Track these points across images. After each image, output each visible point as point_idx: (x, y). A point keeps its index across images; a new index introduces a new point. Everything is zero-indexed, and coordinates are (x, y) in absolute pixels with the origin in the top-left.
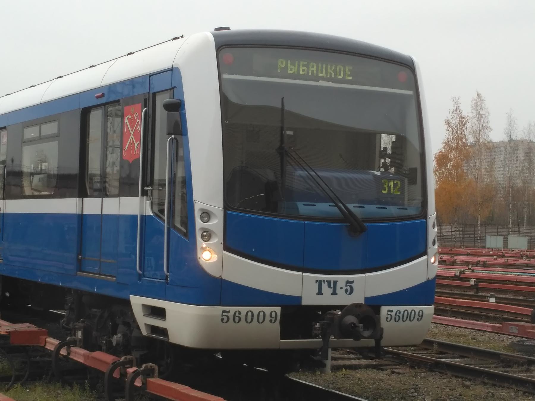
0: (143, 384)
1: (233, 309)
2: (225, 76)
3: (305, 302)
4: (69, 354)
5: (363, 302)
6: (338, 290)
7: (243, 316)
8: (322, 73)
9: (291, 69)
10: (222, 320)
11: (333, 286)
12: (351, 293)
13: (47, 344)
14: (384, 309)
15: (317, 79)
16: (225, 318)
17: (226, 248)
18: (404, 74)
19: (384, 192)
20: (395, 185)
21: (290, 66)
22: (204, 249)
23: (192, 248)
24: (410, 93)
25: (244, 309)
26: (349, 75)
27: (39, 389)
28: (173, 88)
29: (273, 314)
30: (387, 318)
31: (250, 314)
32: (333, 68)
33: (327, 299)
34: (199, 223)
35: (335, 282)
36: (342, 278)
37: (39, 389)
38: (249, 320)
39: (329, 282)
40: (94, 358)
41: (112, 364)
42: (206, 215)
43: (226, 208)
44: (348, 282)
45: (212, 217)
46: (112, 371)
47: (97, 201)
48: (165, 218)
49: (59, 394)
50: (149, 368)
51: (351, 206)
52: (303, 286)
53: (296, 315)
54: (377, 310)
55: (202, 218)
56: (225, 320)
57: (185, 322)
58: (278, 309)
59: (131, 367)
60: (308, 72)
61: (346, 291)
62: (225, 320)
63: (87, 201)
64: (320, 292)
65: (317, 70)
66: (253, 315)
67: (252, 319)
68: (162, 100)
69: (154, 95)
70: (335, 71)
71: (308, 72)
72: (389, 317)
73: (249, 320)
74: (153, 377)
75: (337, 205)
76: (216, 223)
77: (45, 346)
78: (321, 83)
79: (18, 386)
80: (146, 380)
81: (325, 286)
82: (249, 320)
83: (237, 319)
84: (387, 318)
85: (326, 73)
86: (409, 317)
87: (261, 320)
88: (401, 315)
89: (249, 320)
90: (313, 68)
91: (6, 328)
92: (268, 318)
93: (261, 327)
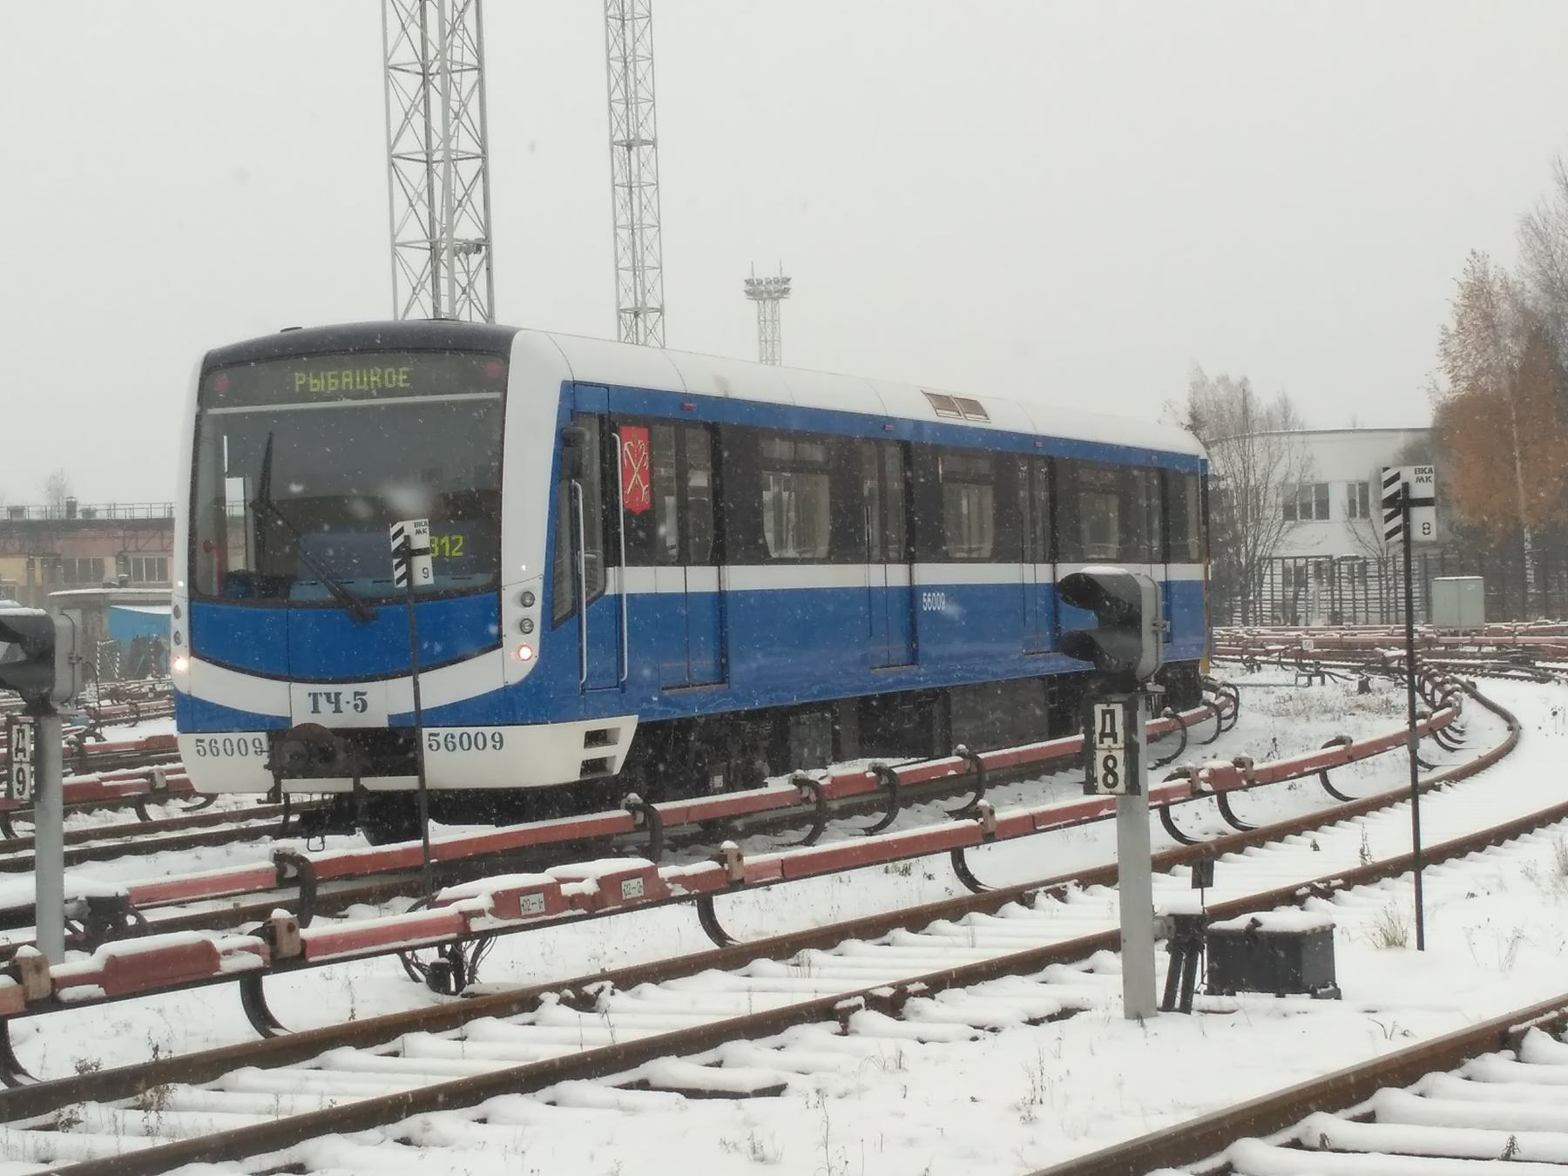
6: (343, 705)
35: (337, 695)
39: (328, 695)
44: (356, 694)
47: (1029, 580)
54: (830, 553)
61: (356, 706)
63: (713, 588)
64: (316, 710)
70: (382, 378)
81: (322, 700)
90: (347, 378)
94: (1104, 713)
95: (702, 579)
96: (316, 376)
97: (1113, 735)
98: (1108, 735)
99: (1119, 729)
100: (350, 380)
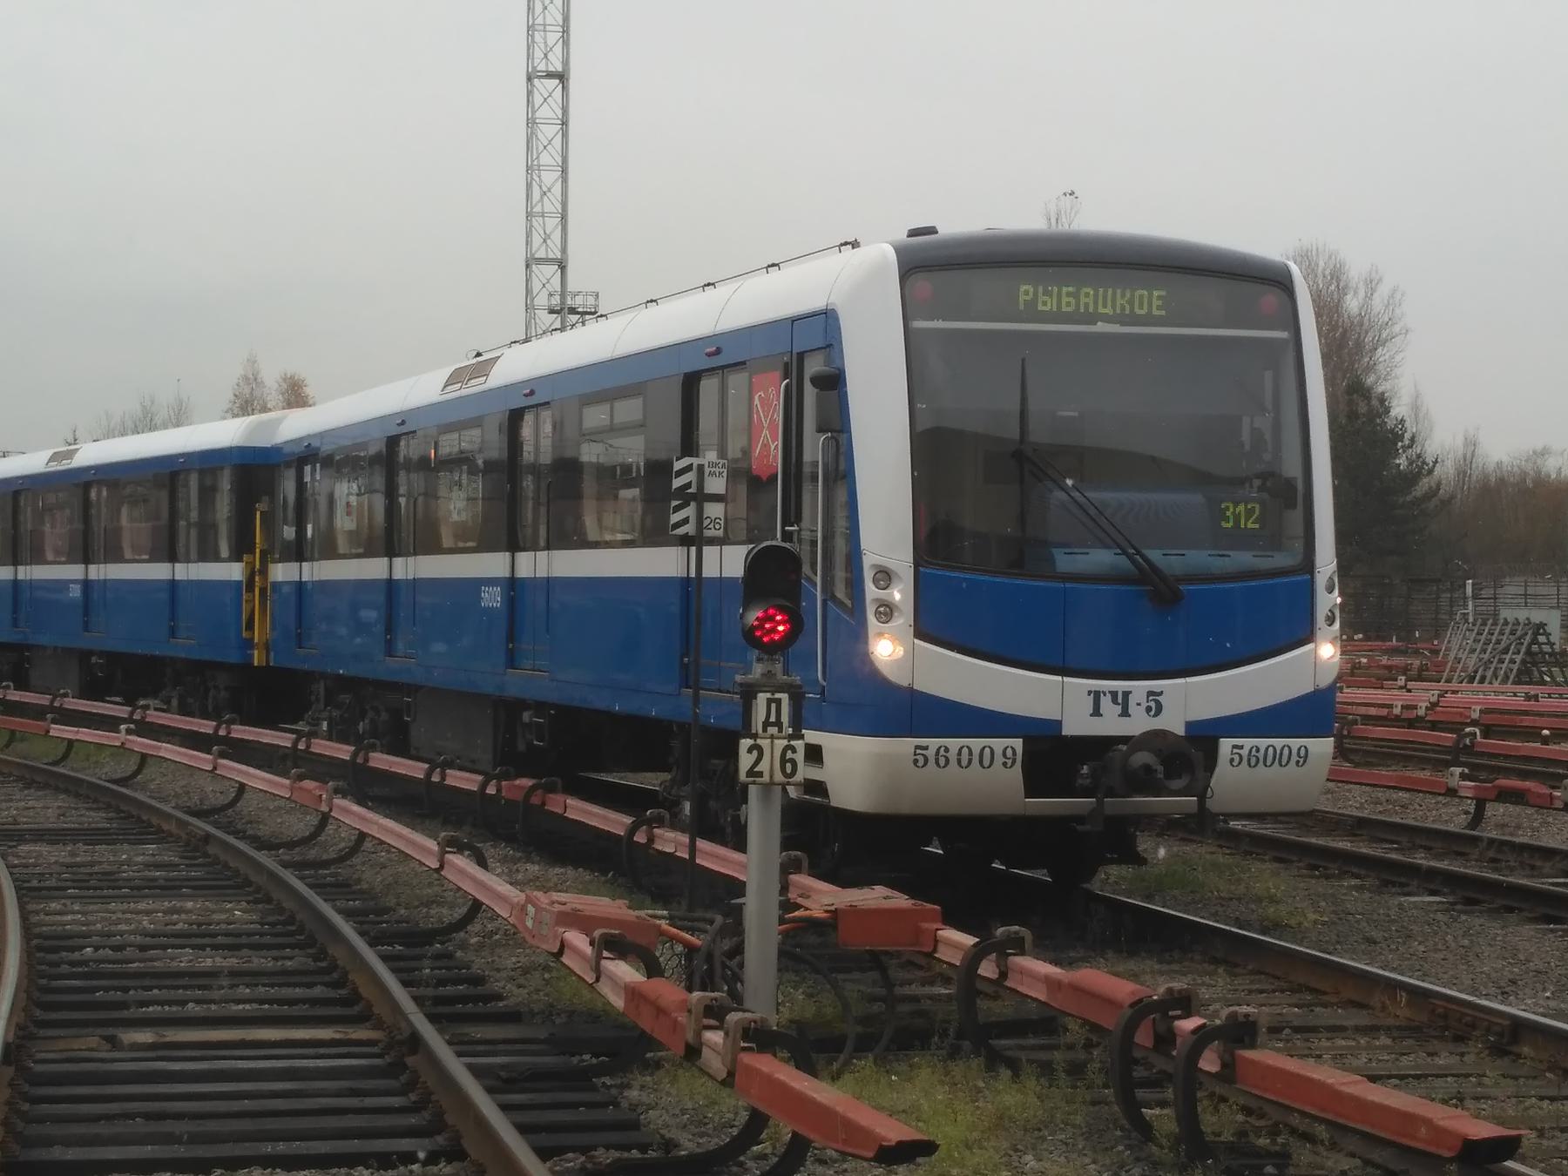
0: (1224, 1065)
1: (933, 743)
2: (919, 324)
3: (1067, 730)
4: (1003, 975)
5: (1180, 730)
6: (1132, 709)
7: (952, 755)
8: (1105, 306)
9: (1045, 303)
10: (916, 761)
11: (1123, 702)
12: (1156, 715)
13: (941, 948)
14: (1226, 744)
15: (1091, 319)
16: (920, 759)
17: (919, 634)
18: (1271, 299)
19: (1224, 525)
20: (1249, 513)
21: (1042, 298)
22: (880, 635)
23: (859, 635)
24: (1284, 335)
25: (954, 743)
26: (1158, 308)
27: (924, 1074)
28: (829, 346)
29: (1009, 752)
30: (1232, 760)
31: (965, 750)
32: (1128, 295)
33: (1110, 724)
34: (871, 591)
35: (1126, 694)
36: (1139, 688)
37: (924, 1074)
38: (964, 763)
39: (1114, 695)
40: (1077, 990)
41: (1132, 1006)
42: (885, 576)
43: (917, 564)
44: (1150, 693)
45: (894, 580)
46: (1130, 1027)
48: (819, 580)
49: (979, 1091)
50: (1241, 1019)
51: (1155, 555)
52: (1068, 702)
53: (1050, 754)
55: (875, 581)
56: (921, 763)
57: (855, 768)
58: (1018, 743)
59: (1187, 1015)
60: (1078, 305)
61: (1149, 709)
62: (921, 763)
64: (1097, 712)
65: (1096, 303)
66: (971, 753)
67: (970, 761)
68: (814, 366)
69: (801, 357)
70: (1131, 302)
71: (1078, 305)
72: (1237, 758)
73: (964, 762)
74: (1253, 1046)
75: (1125, 553)
76: (899, 594)
77: (935, 950)
78: (1101, 327)
79: (866, 1064)
80: (1232, 1055)
81: (1106, 701)
82: (964, 762)
83: (942, 761)
84: (1232, 760)
85: (1114, 307)
86: (1278, 758)
87: (986, 763)
88: (1261, 755)
89: (964, 763)
90: (1088, 295)
91: (826, 901)
92: (999, 759)
93: (988, 777)
94: (769, 701)
95: (159, 571)
96: (1047, 293)
97: (778, 724)
98: (773, 724)
99: (785, 719)
100: (1090, 300)
